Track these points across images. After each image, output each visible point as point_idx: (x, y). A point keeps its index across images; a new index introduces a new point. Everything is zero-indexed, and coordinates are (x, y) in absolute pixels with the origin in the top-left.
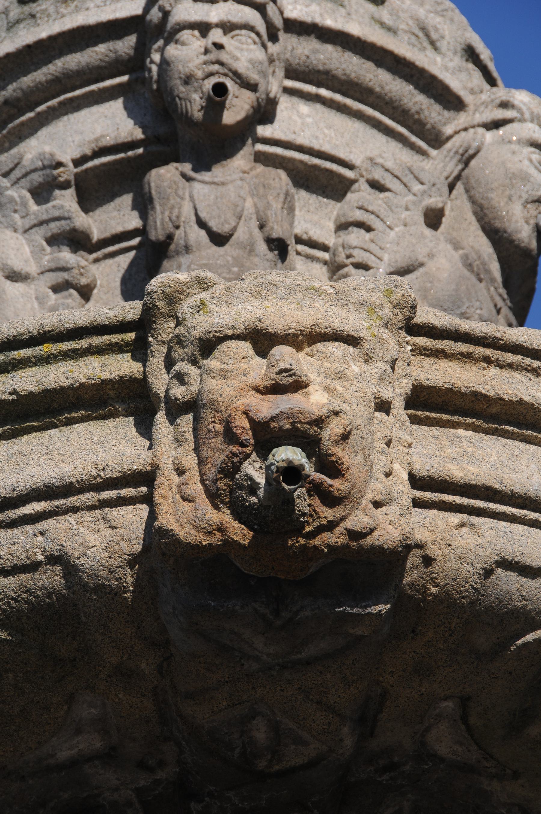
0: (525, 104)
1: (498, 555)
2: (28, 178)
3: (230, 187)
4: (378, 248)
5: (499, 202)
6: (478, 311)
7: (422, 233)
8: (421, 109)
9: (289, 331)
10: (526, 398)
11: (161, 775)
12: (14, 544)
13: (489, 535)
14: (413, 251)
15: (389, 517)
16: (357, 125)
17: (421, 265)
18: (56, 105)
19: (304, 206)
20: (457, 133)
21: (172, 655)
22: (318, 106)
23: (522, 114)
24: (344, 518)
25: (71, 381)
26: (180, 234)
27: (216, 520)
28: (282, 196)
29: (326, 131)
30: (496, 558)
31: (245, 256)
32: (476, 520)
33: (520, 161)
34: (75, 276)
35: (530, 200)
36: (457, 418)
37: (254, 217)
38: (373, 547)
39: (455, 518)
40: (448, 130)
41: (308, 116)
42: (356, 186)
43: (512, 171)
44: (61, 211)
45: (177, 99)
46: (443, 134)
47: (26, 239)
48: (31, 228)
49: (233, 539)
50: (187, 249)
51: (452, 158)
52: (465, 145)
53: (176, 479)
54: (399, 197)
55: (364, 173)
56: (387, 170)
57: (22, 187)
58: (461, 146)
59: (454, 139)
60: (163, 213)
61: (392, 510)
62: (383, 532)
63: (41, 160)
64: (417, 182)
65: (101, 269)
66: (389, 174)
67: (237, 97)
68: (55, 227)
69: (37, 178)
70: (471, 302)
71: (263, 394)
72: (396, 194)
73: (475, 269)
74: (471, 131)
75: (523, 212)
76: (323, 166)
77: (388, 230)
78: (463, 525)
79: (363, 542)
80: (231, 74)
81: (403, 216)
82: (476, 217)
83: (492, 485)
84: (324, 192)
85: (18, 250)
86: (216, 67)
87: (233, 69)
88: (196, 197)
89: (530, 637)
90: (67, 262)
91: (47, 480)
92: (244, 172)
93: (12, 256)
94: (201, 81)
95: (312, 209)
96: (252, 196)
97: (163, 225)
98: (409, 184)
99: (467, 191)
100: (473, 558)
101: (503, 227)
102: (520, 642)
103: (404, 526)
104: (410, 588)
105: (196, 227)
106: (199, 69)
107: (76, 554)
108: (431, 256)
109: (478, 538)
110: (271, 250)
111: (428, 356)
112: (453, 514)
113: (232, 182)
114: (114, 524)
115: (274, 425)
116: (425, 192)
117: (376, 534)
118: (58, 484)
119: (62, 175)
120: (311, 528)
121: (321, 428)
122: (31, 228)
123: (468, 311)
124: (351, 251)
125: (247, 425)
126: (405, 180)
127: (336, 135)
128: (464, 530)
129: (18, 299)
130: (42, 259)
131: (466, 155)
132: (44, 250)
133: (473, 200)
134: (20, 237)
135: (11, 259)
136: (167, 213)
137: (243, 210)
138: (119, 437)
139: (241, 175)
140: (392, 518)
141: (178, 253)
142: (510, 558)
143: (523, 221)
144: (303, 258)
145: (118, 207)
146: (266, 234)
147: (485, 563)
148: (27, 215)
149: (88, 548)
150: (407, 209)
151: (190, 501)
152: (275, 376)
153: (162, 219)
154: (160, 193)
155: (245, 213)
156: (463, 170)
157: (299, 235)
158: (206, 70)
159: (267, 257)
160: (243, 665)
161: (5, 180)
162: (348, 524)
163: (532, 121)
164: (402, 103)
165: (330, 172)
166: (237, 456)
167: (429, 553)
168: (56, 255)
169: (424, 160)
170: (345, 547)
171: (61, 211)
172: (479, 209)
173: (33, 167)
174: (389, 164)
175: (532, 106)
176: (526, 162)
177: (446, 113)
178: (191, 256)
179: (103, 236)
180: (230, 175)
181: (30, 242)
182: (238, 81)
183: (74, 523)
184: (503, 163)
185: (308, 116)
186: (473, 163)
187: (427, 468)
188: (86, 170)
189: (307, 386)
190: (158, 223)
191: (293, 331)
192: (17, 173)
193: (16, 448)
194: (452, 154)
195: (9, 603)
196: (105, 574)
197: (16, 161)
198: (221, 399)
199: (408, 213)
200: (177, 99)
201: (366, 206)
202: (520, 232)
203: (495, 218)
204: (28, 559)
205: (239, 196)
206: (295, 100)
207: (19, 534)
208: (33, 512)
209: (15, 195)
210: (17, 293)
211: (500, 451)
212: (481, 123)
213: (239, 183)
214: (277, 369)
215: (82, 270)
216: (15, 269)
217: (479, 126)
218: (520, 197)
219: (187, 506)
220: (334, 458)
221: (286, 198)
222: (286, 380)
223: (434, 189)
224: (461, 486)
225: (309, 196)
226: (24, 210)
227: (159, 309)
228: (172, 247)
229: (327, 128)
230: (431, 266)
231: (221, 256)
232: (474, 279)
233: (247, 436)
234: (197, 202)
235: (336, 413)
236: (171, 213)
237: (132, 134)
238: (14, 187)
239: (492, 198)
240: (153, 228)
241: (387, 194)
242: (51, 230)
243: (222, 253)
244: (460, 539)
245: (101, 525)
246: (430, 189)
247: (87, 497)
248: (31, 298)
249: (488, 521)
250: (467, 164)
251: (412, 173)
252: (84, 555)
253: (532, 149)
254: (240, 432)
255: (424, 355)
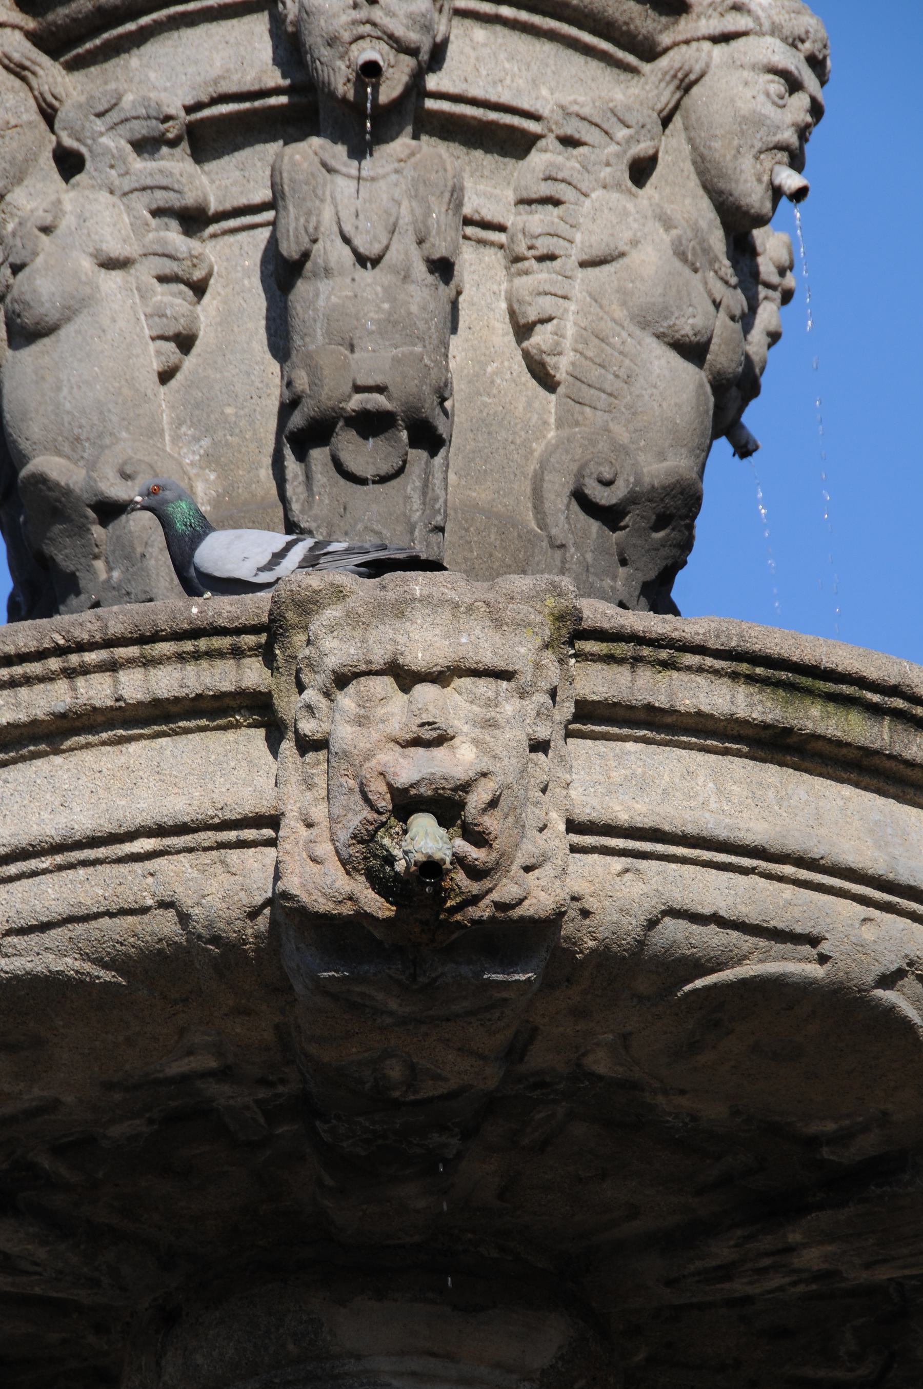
0: (763, 9)
1: (664, 904)
2: (128, 125)
3: (382, 184)
4: (568, 227)
5: (724, 156)
6: (691, 321)
7: (625, 208)
8: (630, 18)
9: (434, 669)
10: (705, 708)
11: (281, 1089)
12: (121, 884)
13: (656, 882)
14: (612, 235)
15: (543, 882)
16: (547, 48)
17: (622, 255)
18: (164, 19)
19: (476, 170)
20: (676, 44)
21: (296, 1000)
22: (499, 28)
23: (761, 25)
24: (490, 890)
25: (186, 691)
26: (319, 250)
27: (348, 889)
28: (447, 195)
29: (507, 65)
30: (663, 907)
31: (398, 283)
32: (643, 864)
33: (754, 97)
34: (186, 269)
35: (764, 149)
36: (625, 731)
37: (411, 228)
38: (522, 918)
39: (618, 864)
40: (665, 39)
41: (485, 45)
42: (542, 143)
43: (742, 112)
44: (170, 180)
45: (318, 62)
46: (659, 45)
47: (124, 204)
48: (132, 191)
49: (365, 911)
50: (328, 272)
51: (668, 84)
52: (686, 68)
53: (303, 832)
54: (597, 151)
55: (554, 127)
56: (584, 119)
57: (120, 136)
58: (680, 68)
59: (671, 53)
60: (297, 219)
61: (546, 872)
62: (534, 901)
63: (145, 108)
64: (622, 125)
65: (218, 247)
66: (586, 123)
67: (392, 67)
68: (161, 199)
69: (141, 129)
70: (681, 310)
71: (403, 747)
72: (593, 147)
73: (690, 257)
74: (694, 45)
75: (754, 168)
76: (502, 121)
77: (582, 198)
78: (627, 871)
79: (510, 913)
80: (385, 38)
81: (602, 175)
82: (696, 169)
83: (660, 826)
84: (502, 148)
85: (114, 225)
86: (368, 28)
87: (389, 32)
88: (339, 197)
89: (699, 983)
90: (177, 250)
91: (159, 818)
92: (401, 161)
93: (109, 238)
94: (347, 46)
95: (486, 173)
96: (410, 197)
97: (297, 237)
98: (611, 131)
99: (686, 129)
100: (637, 909)
101: (728, 188)
102: (688, 988)
103: (558, 891)
104: (565, 941)
105: (339, 241)
106: (346, 30)
107: (190, 902)
108: (635, 243)
109: (643, 886)
110: (431, 272)
111: (595, 661)
112: (616, 858)
113: (384, 176)
114: (233, 870)
115: (413, 792)
116: (631, 137)
117: (526, 903)
118: (170, 823)
119: (171, 129)
120: (453, 903)
121: (467, 793)
122: (132, 191)
123: (677, 322)
124: (534, 241)
125: (383, 788)
126: (605, 126)
127: (520, 70)
128: (628, 876)
129: (116, 295)
130: (144, 236)
131: (687, 81)
132: (147, 225)
133: (690, 140)
134: (118, 202)
135: (107, 242)
136: (302, 220)
137: (397, 219)
138: (240, 756)
139: (396, 165)
140: (545, 883)
141: (315, 275)
142: (678, 907)
143: (754, 178)
144: (473, 243)
145: (241, 166)
146: (426, 253)
147: (650, 914)
148: (127, 173)
149: (203, 897)
150: (608, 164)
151: (318, 863)
152: (417, 729)
153: (296, 229)
154: (293, 189)
155: (401, 222)
156: (681, 98)
157: (469, 216)
158: (355, 32)
159: (426, 282)
160: (375, 1020)
161: (98, 121)
162: (495, 896)
163: (772, 34)
164: (606, 14)
165: (512, 129)
166: (372, 824)
167: (587, 906)
168: (162, 234)
169: (633, 78)
170: (492, 918)
171: (170, 180)
172: (699, 159)
173: (134, 114)
174: (586, 111)
175: (773, 12)
176: (762, 98)
177: (664, 19)
178: (331, 282)
179: (221, 208)
180: (383, 166)
181: (129, 208)
182: (395, 45)
183: (187, 865)
184: (732, 101)
185: (485, 45)
186: (695, 90)
187: (588, 811)
188: (202, 120)
189: (452, 738)
190: (291, 234)
191: (439, 668)
192: (114, 117)
193: (123, 759)
194: (668, 78)
195: (114, 946)
196: (222, 925)
197: (113, 101)
198: (356, 752)
199: (608, 169)
200: (318, 62)
201: (554, 175)
202: (750, 195)
203: (719, 177)
204: (137, 903)
205: (393, 200)
206: (468, 22)
207: (126, 873)
208: (142, 851)
209: (112, 145)
210: (114, 286)
211: (674, 769)
212: (706, 35)
213: (394, 177)
214: (419, 721)
215: (195, 260)
216: (112, 255)
217: (704, 38)
218: (752, 146)
219: (315, 868)
220: (479, 829)
221: (452, 195)
222: (427, 734)
223: (644, 131)
224: (626, 829)
225: (483, 156)
226: (123, 166)
227: (287, 621)
228: (309, 265)
229: (508, 60)
230: (635, 257)
231: (369, 285)
232: (687, 271)
233: (385, 803)
234: (340, 208)
235: (484, 775)
236: (307, 221)
237: (260, 80)
238: (111, 133)
239: (716, 150)
240: (285, 235)
241: (581, 150)
242: (156, 200)
243: (369, 280)
244: (623, 887)
245: (219, 868)
246: (637, 133)
247: (202, 837)
248: (131, 290)
249: (654, 863)
250: (687, 89)
251: (615, 115)
252: (198, 904)
253: (771, 77)
254: (375, 797)
255: (591, 660)
